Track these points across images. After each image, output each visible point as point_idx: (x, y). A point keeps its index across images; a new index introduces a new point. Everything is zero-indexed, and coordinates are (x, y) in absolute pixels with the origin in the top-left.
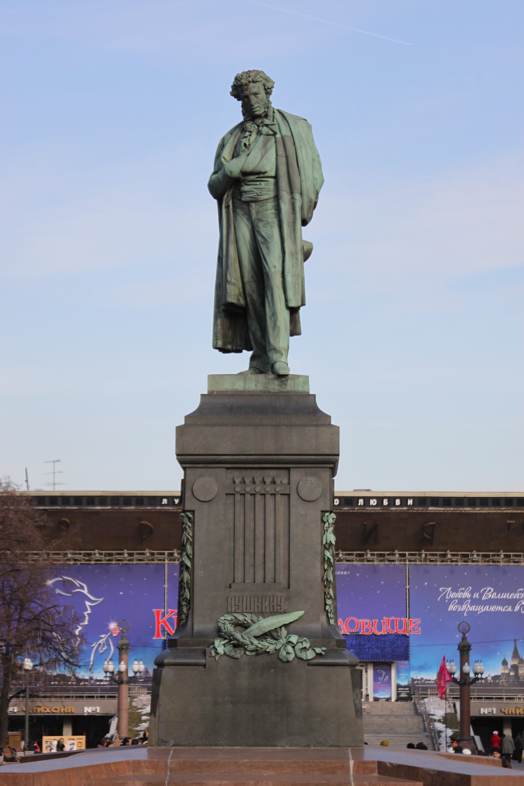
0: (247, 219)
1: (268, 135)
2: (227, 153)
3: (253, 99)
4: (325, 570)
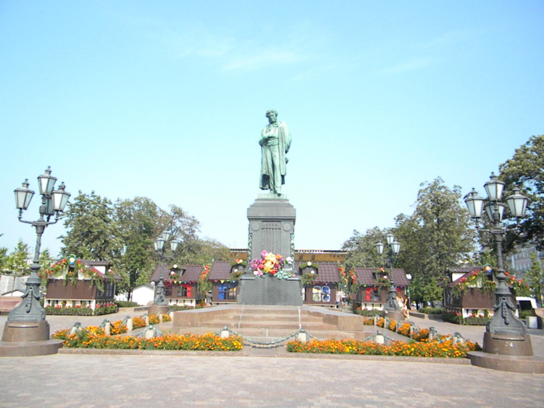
2: (264, 132)
3: (272, 117)
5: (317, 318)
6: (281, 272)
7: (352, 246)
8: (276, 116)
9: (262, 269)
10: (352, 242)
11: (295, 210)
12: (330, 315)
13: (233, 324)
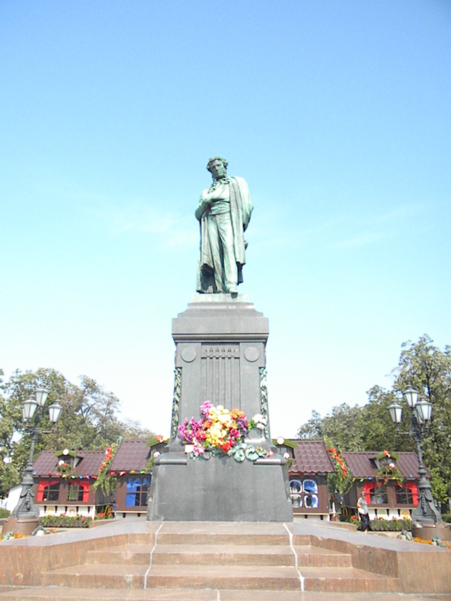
1: (225, 184)
4: (262, 403)
5: (339, 555)
6: (244, 446)
7: (311, 431)
8: (225, 167)
9: (202, 439)
10: (311, 426)
11: (267, 320)
12: (374, 549)
13: (129, 577)
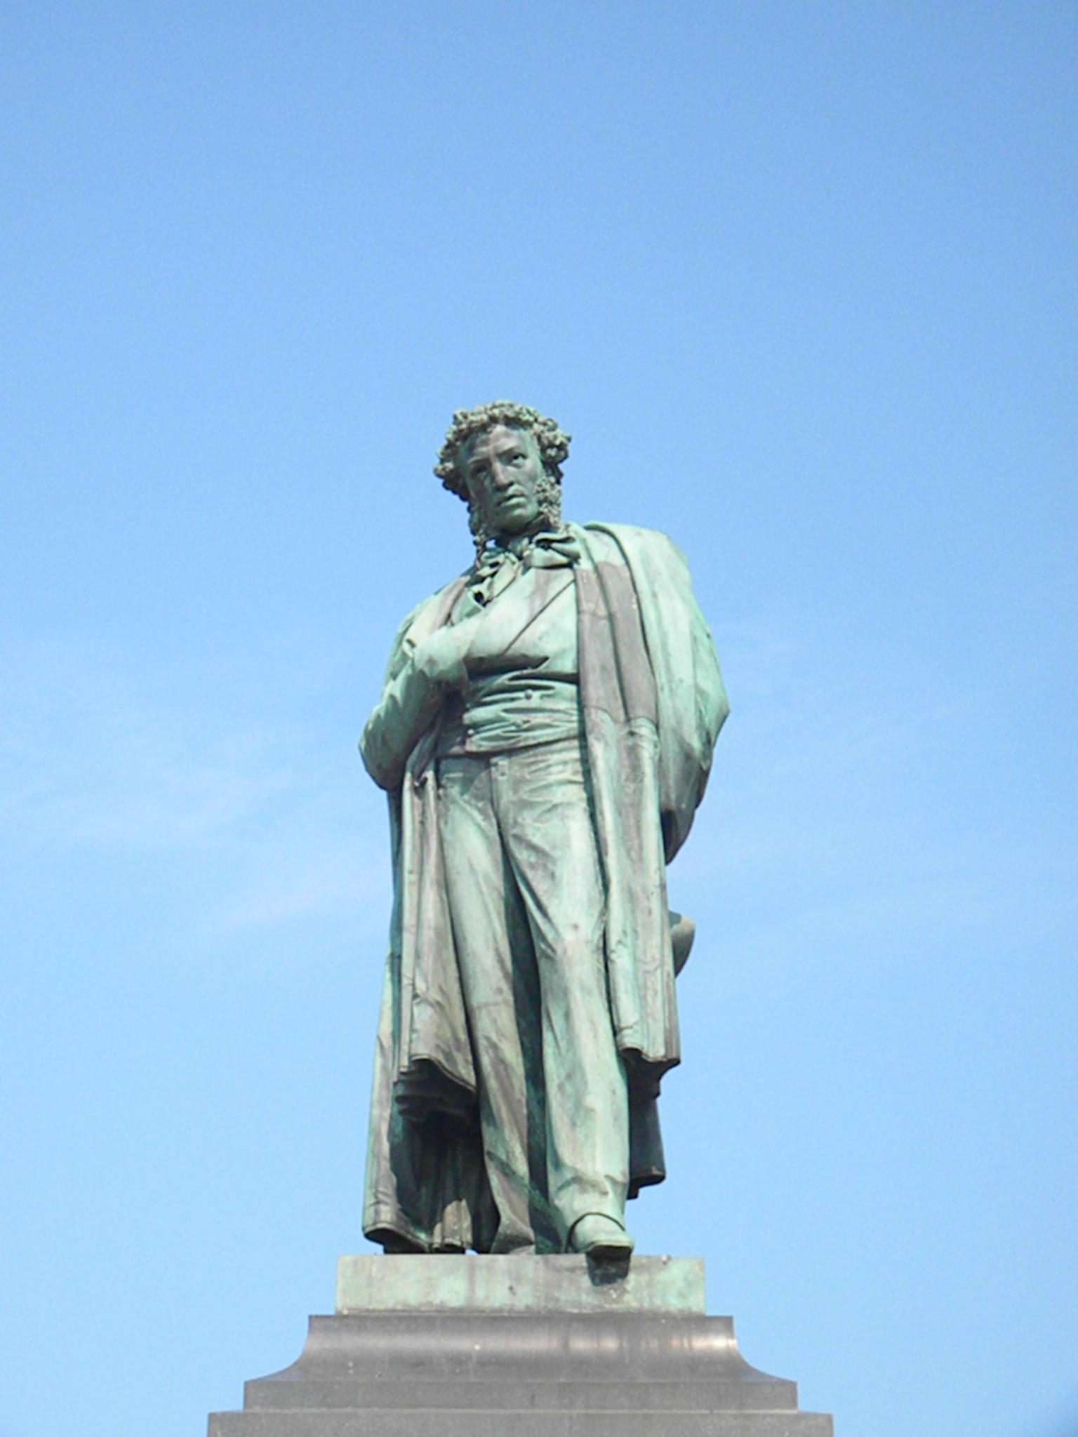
0: (482, 811)
8: (552, 466)
